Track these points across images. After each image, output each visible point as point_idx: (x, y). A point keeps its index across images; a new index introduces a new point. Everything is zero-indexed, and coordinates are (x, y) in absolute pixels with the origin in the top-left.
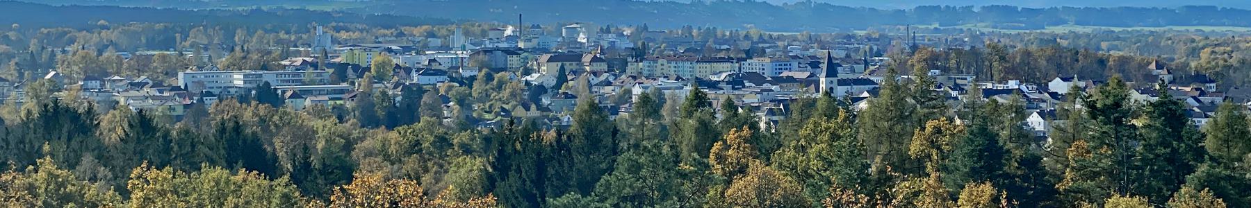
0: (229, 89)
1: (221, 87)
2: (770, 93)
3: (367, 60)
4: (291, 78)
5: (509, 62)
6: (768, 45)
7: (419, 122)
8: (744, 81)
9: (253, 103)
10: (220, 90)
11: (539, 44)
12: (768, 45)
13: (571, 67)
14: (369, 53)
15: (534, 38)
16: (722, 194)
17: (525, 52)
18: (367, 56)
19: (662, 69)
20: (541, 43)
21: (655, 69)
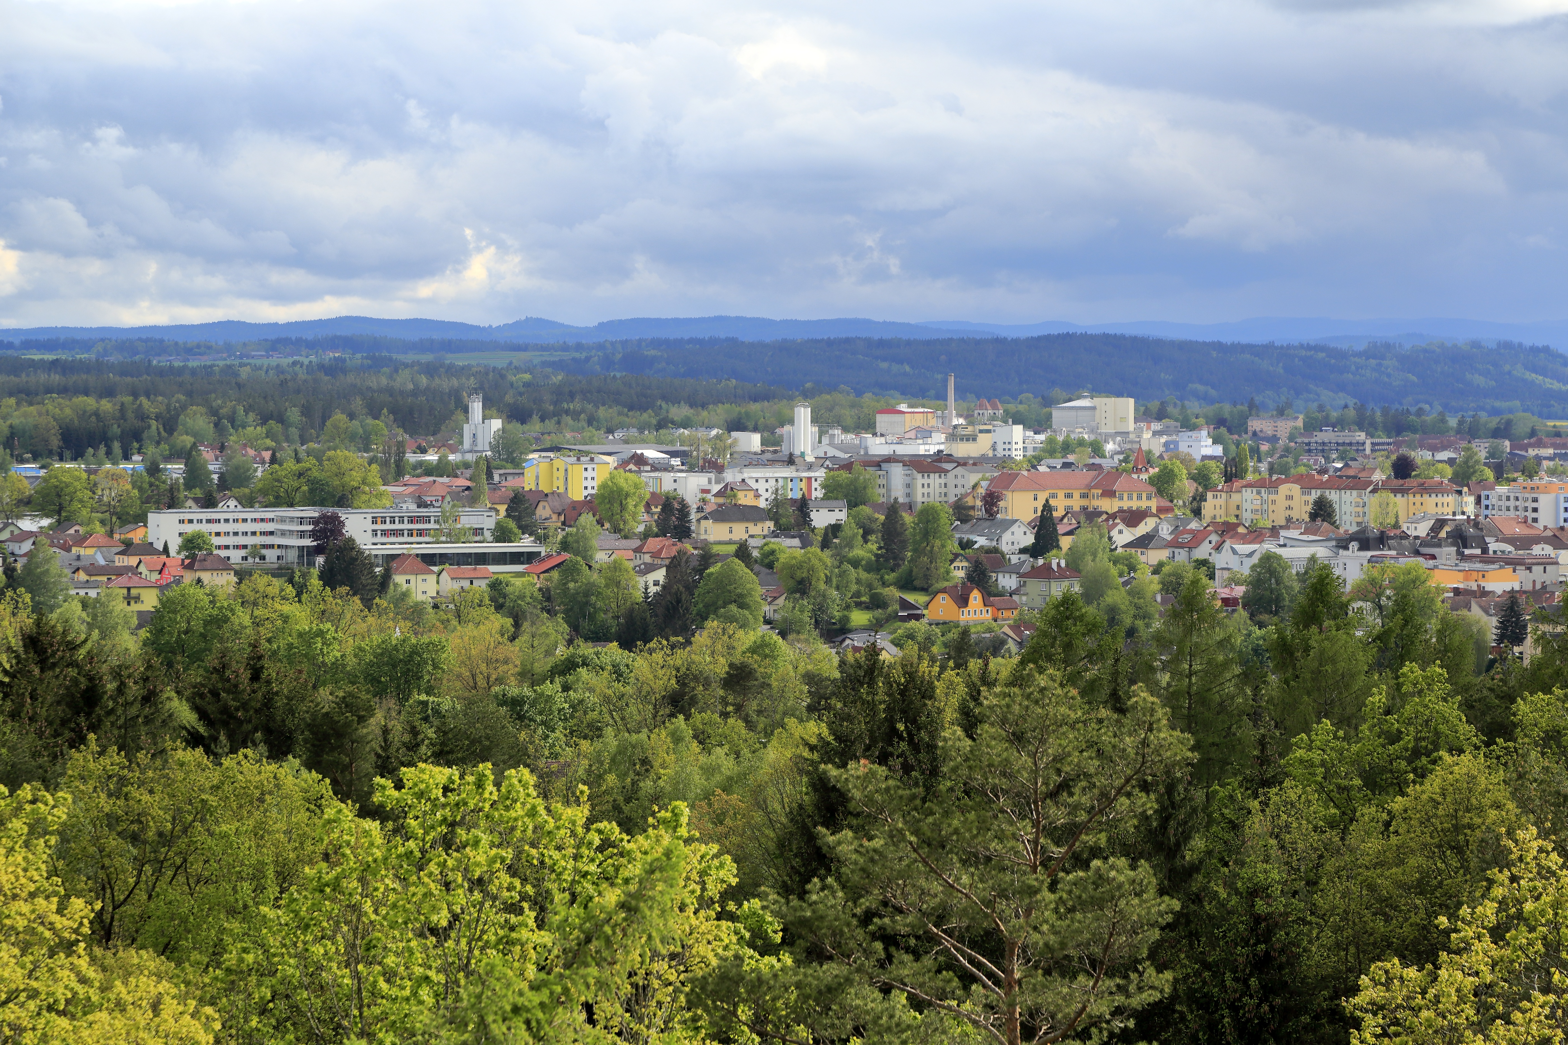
0: (264, 552)
1: (245, 547)
2: (1548, 568)
3: (585, 484)
4: (406, 526)
5: (920, 491)
6: (1551, 451)
7: (833, 834)
8: (1488, 539)
9: (731, 476)
10: (243, 553)
11: (994, 447)
12: (1551, 451)
13: (1069, 502)
14: (590, 467)
15: (981, 431)
16: (1406, 772)
17: (959, 464)
18: (585, 474)
19: (1289, 508)
20: (1000, 447)
21: (1271, 508)
